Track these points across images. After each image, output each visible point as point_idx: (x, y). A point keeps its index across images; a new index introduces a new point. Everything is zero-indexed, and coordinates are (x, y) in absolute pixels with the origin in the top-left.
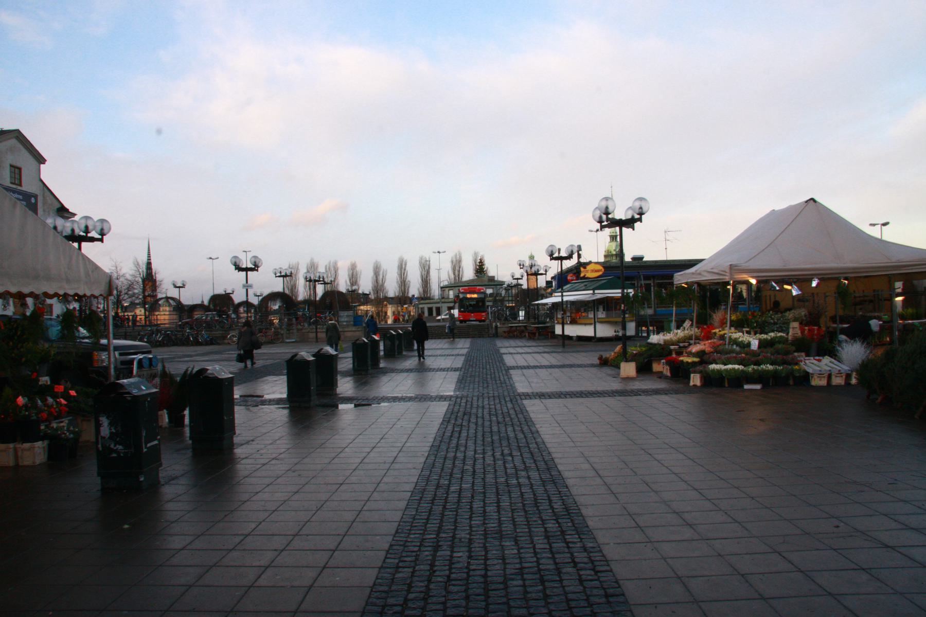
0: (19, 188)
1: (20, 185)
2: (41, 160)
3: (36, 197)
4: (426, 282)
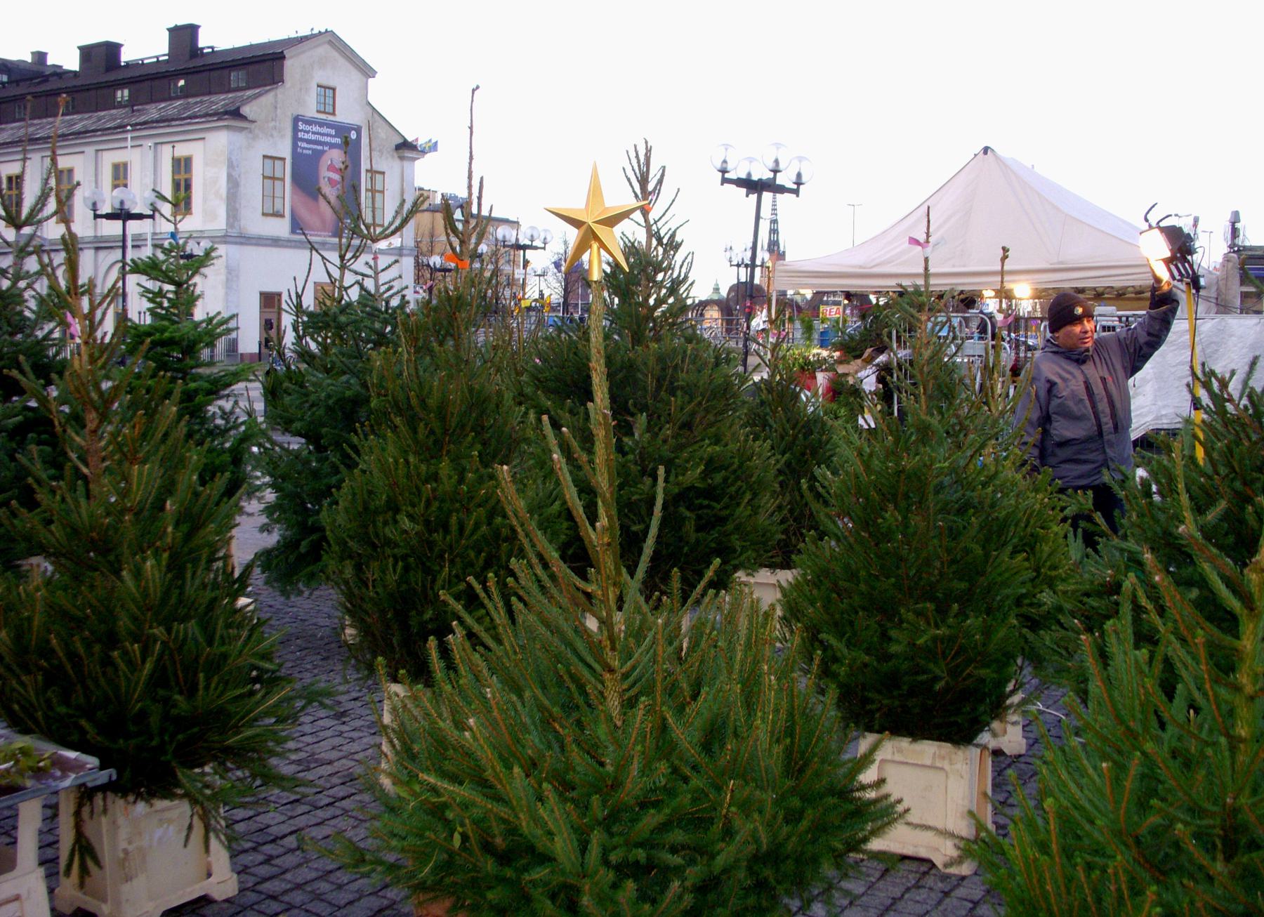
0: (331, 118)
1: (333, 114)
2: (367, 72)
3: (358, 130)
4: (269, 326)
